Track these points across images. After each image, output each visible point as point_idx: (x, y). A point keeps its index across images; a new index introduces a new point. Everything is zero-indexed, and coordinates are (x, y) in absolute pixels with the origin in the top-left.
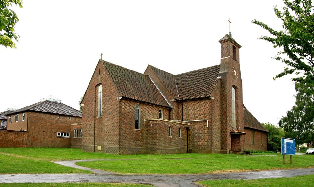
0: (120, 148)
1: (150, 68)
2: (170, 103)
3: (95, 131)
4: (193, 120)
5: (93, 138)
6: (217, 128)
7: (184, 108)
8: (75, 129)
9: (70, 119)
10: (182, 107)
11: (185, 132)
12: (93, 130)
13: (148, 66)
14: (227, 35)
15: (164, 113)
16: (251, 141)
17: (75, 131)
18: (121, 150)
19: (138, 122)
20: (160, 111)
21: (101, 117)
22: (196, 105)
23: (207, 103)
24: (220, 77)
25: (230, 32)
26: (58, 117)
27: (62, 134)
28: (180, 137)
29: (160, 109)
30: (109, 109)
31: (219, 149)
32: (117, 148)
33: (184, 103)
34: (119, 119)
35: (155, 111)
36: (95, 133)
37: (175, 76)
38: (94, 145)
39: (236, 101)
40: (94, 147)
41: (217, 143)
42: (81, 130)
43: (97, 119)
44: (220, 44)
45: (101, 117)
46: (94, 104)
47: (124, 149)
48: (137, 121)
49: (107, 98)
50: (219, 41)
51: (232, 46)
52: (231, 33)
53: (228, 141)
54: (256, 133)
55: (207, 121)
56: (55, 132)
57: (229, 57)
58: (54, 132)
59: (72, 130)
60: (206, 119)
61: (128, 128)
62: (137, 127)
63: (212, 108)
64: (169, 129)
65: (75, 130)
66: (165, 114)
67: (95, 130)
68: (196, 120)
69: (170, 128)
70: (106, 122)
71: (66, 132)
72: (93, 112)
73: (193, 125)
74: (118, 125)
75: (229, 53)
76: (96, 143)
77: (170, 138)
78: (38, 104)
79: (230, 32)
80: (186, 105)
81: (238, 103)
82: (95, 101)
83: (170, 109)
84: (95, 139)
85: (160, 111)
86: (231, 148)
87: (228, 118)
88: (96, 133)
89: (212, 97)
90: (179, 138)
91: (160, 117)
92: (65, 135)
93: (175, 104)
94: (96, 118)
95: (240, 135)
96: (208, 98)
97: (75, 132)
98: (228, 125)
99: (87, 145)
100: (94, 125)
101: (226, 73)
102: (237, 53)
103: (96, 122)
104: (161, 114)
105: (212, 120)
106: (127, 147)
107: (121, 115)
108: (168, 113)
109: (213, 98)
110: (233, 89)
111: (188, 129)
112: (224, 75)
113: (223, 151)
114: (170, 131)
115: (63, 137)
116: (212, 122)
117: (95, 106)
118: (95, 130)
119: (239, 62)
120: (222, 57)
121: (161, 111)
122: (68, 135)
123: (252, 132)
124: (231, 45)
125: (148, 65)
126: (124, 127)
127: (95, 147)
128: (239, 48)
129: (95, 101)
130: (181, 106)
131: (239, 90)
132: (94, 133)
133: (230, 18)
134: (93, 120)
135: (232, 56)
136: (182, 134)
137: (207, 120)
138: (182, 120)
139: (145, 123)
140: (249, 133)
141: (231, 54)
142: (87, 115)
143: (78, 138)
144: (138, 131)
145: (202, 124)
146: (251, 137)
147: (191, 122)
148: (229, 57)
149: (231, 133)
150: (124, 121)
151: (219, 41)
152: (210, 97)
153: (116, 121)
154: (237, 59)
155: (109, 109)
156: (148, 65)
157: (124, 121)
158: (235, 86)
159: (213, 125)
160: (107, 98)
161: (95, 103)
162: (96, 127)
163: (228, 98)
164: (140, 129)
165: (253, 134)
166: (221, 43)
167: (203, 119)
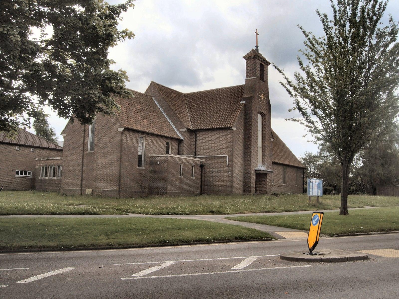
0: (119, 191)
1: (154, 86)
2: (181, 133)
3: (82, 170)
4: (210, 155)
5: (80, 179)
6: (239, 165)
7: (198, 139)
8: (42, 166)
9: (34, 151)
10: (196, 139)
11: (199, 170)
12: (80, 168)
13: (151, 84)
14: (253, 50)
15: (173, 146)
16: (282, 181)
17: (43, 168)
18: (120, 194)
19: (141, 158)
20: (167, 144)
21: (93, 151)
22: (214, 136)
23: (226, 134)
24: (244, 102)
25: (257, 47)
26: (18, 148)
27: (21, 173)
28: (192, 176)
29: (168, 141)
30: (106, 142)
31: (240, 190)
32: (116, 191)
33: (198, 133)
34: (119, 155)
35: (162, 144)
36: (82, 173)
37: (185, 95)
38: (81, 188)
39: (263, 131)
40: (81, 190)
41: (238, 184)
42: (61, 167)
43: (87, 154)
44: (244, 61)
45: (93, 151)
46: (83, 135)
47: (124, 193)
48: (140, 157)
49: (104, 127)
50: (244, 57)
51: (259, 64)
52: (259, 48)
53: (252, 181)
54: (289, 169)
55: (227, 156)
56: (13, 170)
57: (255, 77)
58: (12, 169)
59: (37, 167)
60: (225, 155)
61: (130, 166)
62: (140, 165)
63: (233, 141)
64: (179, 167)
65: (42, 168)
66: (174, 147)
67: (82, 168)
68: (213, 155)
69: (181, 165)
70: (101, 159)
71: (27, 170)
72: (81, 145)
73: (209, 162)
74: (119, 163)
75: (255, 72)
76: (84, 186)
77: (180, 178)
78: (376, 244)
79: (257, 47)
80: (200, 136)
81: (265, 133)
82: (85, 131)
83: (180, 141)
84: (82, 180)
85: (167, 144)
86: (256, 190)
87: (252, 153)
88: (85, 172)
89: (235, 127)
90: (192, 178)
91: (167, 152)
92: (26, 174)
93: (187, 135)
94: (85, 153)
95: (267, 173)
96: (229, 128)
97: (42, 170)
98: (252, 161)
99: (70, 188)
100: (81, 162)
101: (250, 97)
102: (265, 72)
103: (85, 157)
104: (169, 147)
105: (233, 156)
106: (127, 190)
107: (121, 149)
108: (177, 146)
109: (234, 129)
110: (260, 116)
111: (202, 166)
112: (249, 99)
113: (246, 191)
114: (180, 170)
115: (23, 177)
116: (232, 158)
117: (84, 137)
118: (82, 168)
119: (267, 83)
120: (246, 77)
121: (168, 143)
122: (29, 173)
123: (283, 167)
124: (258, 62)
125: (152, 81)
126: (125, 166)
127: (82, 192)
128: (268, 65)
129: (85, 131)
130: (194, 137)
131: (266, 117)
132: (81, 172)
133: (257, 30)
134: (81, 156)
135: (259, 76)
136: (195, 172)
137: (227, 156)
138: (195, 155)
139: (149, 160)
140: (280, 169)
141: (258, 73)
142: (71, 148)
143: (47, 178)
144: (141, 170)
145: (220, 161)
146: (282, 176)
147: (206, 157)
148: (255, 77)
149: (256, 172)
150: (126, 157)
151: (244, 57)
152: (231, 127)
153: (116, 157)
154: (265, 80)
155: (106, 142)
156: (152, 81)
157: (126, 157)
158: (263, 113)
159: (235, 162)
160: (104, 127)
161: (84, 134)
162: (84, 164)
163: (253, 128)
164: (143, 168)
165: (285, 172)
166: (246, 59)
167: (222, 154)
